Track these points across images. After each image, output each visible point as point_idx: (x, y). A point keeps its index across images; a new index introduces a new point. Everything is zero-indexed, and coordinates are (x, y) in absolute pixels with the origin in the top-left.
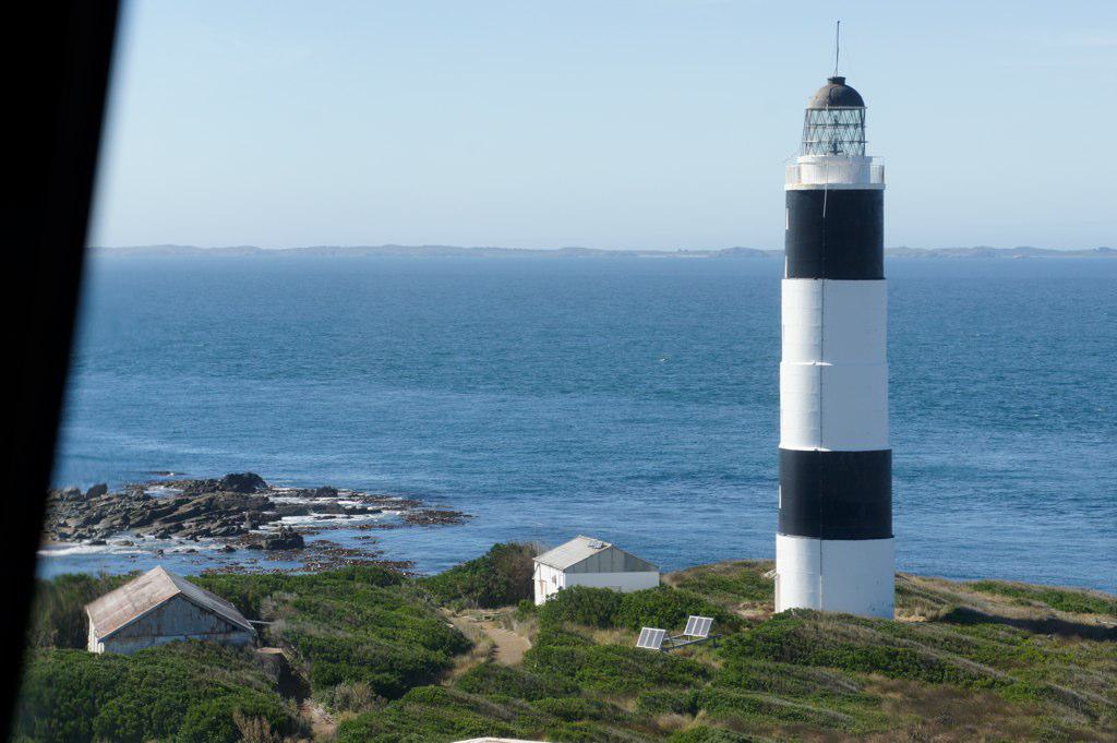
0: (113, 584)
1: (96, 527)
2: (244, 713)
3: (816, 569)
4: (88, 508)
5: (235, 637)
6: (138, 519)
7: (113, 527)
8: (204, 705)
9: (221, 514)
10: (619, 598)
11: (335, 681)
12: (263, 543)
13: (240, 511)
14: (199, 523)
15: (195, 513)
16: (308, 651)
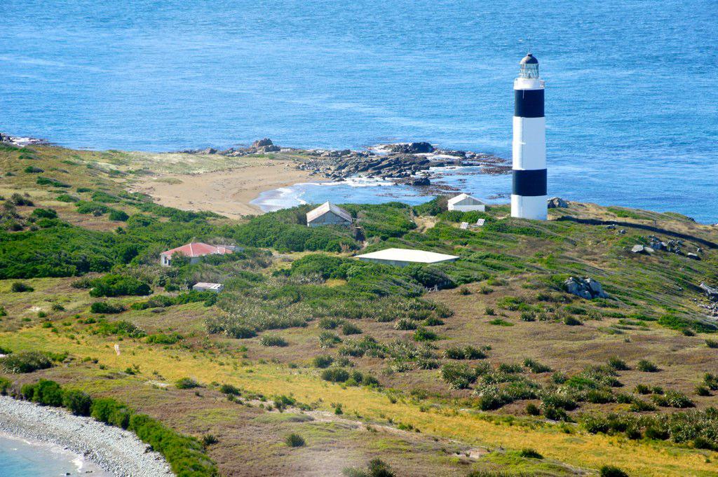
0: (315, 207)
1: (343, 171)
2: (343, 244)
3: (521, 204)
4: (341, 161)
5: (346, 223)
6: (362, 168)
7: (350, 171)
8: (333, 241)
9: (401, 166)
10: (463, 213)
11: (372, 236)
12: (411, 182)
13: (411, 164)
14: (390, 170)
15: (389, 165)
16: (365, 227)
